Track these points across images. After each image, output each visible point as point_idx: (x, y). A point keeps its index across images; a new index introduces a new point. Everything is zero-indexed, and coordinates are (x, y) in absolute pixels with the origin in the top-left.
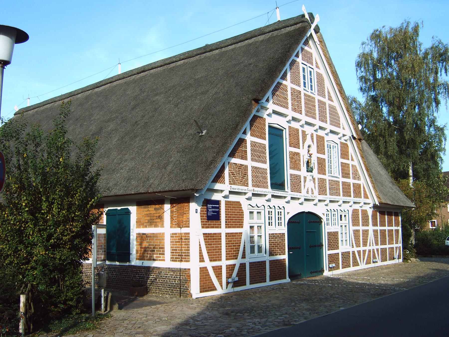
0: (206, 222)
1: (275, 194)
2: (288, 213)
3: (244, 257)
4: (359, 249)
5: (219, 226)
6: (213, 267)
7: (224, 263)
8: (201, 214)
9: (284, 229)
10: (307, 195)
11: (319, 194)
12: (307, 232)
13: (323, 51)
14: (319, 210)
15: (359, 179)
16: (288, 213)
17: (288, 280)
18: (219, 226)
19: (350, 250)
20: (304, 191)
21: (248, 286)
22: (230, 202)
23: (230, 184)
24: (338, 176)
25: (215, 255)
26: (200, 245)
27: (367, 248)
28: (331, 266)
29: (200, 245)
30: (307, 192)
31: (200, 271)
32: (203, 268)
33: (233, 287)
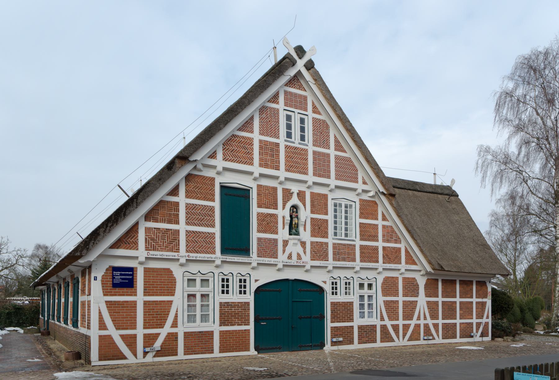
0: (110, 289)
1: (261, 262)
3: (419, 318)
4: (426, 322)
6: (392, 325)
7: (440, 321)
8: (102, 281)
9: (250, 298)
10: (290, 261)
11: (312, 260)
12: (293, 301)
13: (321, 90)
14: (316, 278)
15: (398, 241)
16: (256, 281)
17: (252, 352)
19: (378, 323)
22: (149, 268)
23: (146, 250)
24: (354, 239)
25: (434, 316)
26: (177, 311)
28: (334, 340)
29: (177, 311)
31: (144, 337)
32: (384, 325)
33: (154, 356)
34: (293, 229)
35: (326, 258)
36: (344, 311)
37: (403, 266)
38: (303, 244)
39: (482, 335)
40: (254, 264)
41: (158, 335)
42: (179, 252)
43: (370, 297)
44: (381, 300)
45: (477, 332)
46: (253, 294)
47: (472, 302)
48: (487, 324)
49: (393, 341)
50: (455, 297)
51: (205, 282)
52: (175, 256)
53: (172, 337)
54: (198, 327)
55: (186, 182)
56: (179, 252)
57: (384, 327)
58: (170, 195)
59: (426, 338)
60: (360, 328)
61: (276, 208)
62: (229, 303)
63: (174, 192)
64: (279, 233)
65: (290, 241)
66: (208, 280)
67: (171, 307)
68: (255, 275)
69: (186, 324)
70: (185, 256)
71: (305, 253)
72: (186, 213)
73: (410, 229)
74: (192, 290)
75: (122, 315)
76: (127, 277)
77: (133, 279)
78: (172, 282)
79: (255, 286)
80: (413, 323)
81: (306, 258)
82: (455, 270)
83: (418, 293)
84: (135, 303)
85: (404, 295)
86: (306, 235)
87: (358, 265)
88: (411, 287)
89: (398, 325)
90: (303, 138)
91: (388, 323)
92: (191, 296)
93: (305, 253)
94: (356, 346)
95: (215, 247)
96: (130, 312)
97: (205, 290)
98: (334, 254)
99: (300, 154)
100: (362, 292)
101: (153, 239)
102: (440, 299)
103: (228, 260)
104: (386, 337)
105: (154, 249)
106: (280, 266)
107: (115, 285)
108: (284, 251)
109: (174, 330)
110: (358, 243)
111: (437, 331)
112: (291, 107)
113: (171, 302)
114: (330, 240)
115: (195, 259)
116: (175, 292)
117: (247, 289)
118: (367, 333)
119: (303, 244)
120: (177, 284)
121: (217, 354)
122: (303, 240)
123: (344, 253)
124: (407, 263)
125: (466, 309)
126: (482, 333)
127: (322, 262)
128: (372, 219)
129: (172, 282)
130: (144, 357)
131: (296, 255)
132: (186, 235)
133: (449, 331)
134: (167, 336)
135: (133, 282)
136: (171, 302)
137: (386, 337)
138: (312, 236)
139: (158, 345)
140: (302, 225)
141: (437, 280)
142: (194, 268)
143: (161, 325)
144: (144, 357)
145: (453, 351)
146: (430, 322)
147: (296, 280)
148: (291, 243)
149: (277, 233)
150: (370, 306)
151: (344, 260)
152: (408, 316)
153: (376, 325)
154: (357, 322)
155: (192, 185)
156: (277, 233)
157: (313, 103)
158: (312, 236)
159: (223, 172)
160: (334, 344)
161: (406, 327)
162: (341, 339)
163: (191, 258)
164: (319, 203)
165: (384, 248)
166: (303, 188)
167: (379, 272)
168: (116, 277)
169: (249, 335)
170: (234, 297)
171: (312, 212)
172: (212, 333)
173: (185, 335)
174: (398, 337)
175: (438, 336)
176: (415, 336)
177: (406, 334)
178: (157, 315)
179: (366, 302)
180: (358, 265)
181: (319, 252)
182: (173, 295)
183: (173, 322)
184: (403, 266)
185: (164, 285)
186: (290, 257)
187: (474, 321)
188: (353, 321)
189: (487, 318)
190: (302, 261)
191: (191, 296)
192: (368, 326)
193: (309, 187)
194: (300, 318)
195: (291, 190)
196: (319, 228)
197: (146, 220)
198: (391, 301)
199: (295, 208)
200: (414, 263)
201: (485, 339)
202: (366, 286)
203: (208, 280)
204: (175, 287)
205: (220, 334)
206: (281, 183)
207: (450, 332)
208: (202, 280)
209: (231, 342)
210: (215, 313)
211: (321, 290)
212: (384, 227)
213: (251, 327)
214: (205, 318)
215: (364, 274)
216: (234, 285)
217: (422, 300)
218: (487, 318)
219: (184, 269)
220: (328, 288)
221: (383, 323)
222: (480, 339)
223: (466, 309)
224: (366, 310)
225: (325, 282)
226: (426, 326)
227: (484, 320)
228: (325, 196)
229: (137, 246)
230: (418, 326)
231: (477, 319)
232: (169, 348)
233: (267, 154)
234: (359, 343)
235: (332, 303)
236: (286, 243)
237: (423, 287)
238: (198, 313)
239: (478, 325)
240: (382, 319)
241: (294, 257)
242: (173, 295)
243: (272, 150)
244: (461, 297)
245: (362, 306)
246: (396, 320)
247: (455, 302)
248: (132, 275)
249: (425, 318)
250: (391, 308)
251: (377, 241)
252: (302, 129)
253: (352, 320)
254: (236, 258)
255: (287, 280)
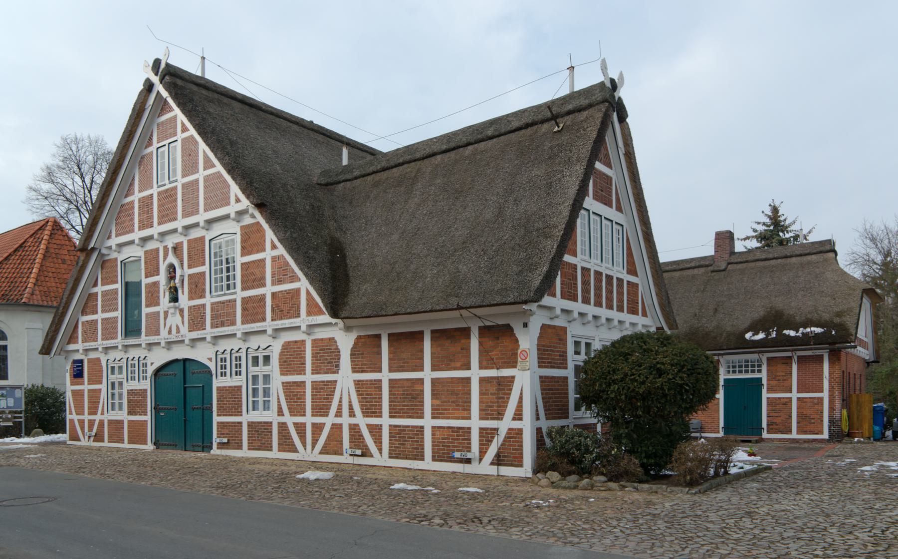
2: (152, 364)
3: (339, 413)
4: (353, 421)
5: (83, 384)
7: (386, 421)
9: (146, 385)
10: (170, 336)
14: (203, 354)
17: (150, 447)
18: (83, 384)
20: (164, 333)
21: (106, 444)
25: (371, 408)
26: (521, 394)
27: (98, 418)
29: (521, 394)
30: (170, 332)
32: (355, 425)
36: (232, 400)
49: (295, 450)
53: (515, 436)
57: (283, 426)
71: (183, 323)
79: (151, 370)
80: (329, 421)
83: (338, 366)
85: (315, 371)
89: (304, 425)
92: (255, 378)
93: (183, 323)
100: (253, 370)
102: (385, 376)
104: (286, 444)
111: (378, 442)
118: (260, 435)
122: (181, 307)
126: (498, 455)
133: (406, 443)
137: (286, 444)
141: (378, 337)
145: (374, 487)
146: (362, 421)
150: (266, 392)
152: (321, 409)
153: (271, 423)
161: (318, 428)
174: (305, 446)
175: (380, 450)
177: (317, 440)
179: (260, 386)
183: (516, 410)
192: (260, 423)
194: (193, 409)
198: (294, 382)
201: (508, 471)
207: (408, 445)
214: (266, 407)
217: (346, 379)
221: (282, 419)
222: (493, 470)
224: (261, 399)
225: (210, 359)
226: (355, 430)
237: (349, 352)
241: (174, 331)
249: (352, 414)
250: (293, 392)
253: (239, 413)
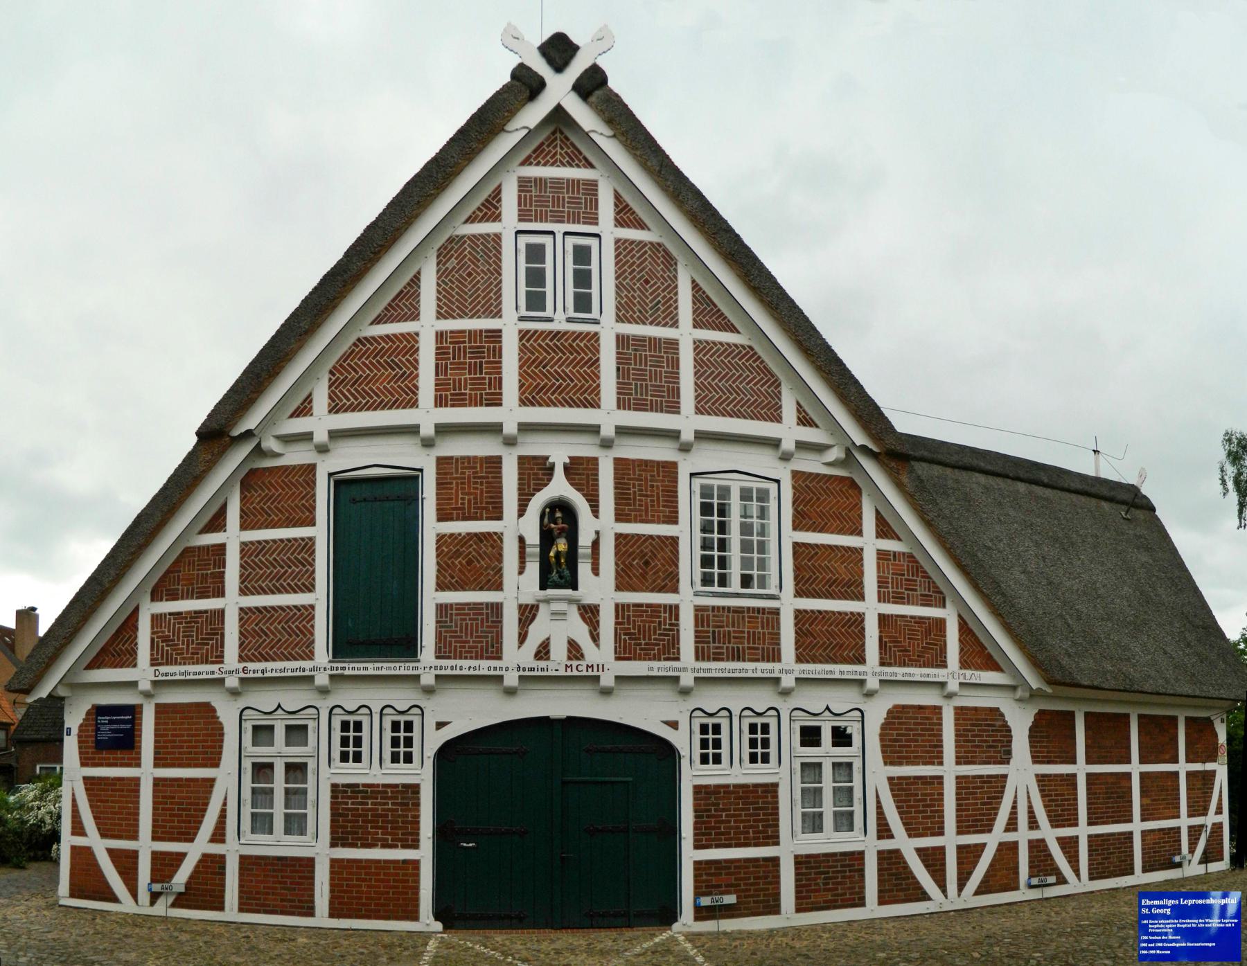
3: (1012, 825)
7: (1083, 831)
8: (79, 736)
9: (422, 774)
10: (542, 664)
11: (618, 659)
14: (643, 712)
15: (936, 596)
17: (427, 921)
19: (871, 846)
23: (152, 665)
25: (1062, 814)
26: (225, 804)
28: (705, 901)
34: (559, 570)
35: (670, 651)
36: (749, 812)
37: (952, 672)
38: (590, 614)
39: (1205, 860)
40: (428, 679)
41: (181, 856)
42: (222, 662)
43: (843, 768)
44: (878, 774)
45: (1192, 851)
46: (429, 764)
47: (1176, 774)
48: (1218, 827)
49: (924, 896)
50: (1128, 761)
51: (297, 733)
52: (212, 673)
54: (278, 844)
55: (242, 493)
56: (222, 662)
58: (207, 532)
59: (1035, 881)
60: (802, 862)
61: (496, 513)
62: (357, 785)
63: (217, 522)
64: (505, 586)
65: (542, 607)
66: (305, 727)
67: (211, 792)
68: (436, 708)
69: (248, 836)
70: (237, 671)
71: (595, 638)
72: (242, 566)
73: (966, 561)
74: (263, 753)
75: (114, 807)
76: (122, 726)
77: (133, 729)
78: (215, 735)
79: (434, 741)
80: (992, 840)
81: (601, 654)
82: (1112, 684)
83: (1009, 753)
84: (136, 781)
86: (599, 586)
87: (791, 672)
88: (982, 733)
89: (941, 850)
90: (583, 303)
91: (907, 845)
92: (262, 770)
93: (595, 638)
94: (789, 916)
95: (313, 642)
96: (127, 802)
97: (296, 753)
98: (699, 638)
99: (572, 349)
101: (166, 639)
102: (1081, 769)
103: (347, 672)
105: (169, 662)
106: (511, 679)
107: (100, 745)
108: (522, 638)
109: (216, 849)
110: (789, 604)
111: (1073, 860)
112: (541, 218)
113: (211, 782)
114: (688, 598)
115: (260, 675)
116: (220, 759)
117: (415, 750)
118: (829, 879)
119: (590, 614)
120: (226, 738)
121: (322, 918)
122: (589, 600)
123: (737, 636)
124: (965, 664)
125: (1160, 795)
126: (1205, 853)
127: (655, 664)
128: (840, 531)
129: (215, 735)
130: (152, 903)
131: (565, 646)
132: (241, 619)
133: (1111, 855)
134: (200, 861)
135: (133, 735)
136: (211, 782)
137: (898, 883)
138: (619, 588)
139: (181, 877)
140: (585, 556)
142: (264, 700)
143: (189, 834)
144: (152, 903)
146: (1050, 834)
147: (570, 719)
148: (543, 612)
149: (499, 587)
151: (736, 656)
154: (793, 844)
155: (256, 495)
156: (499, 587)
157: (617, 197)
158: (619, 588)
159: (334, 442)
160: (702, 913)
161: (969, 856)
162: (730, 899)
163: (251, 675)
164: (646, 489)
165: (883, 619)
166: (583, 448)
167: (869, 695)
168: (102, 728)
169: (418, 875)
170: (376, 771)
171: (620, 517)
172: (309, 863)
173: (241, 863)
176: (1002, 875)
177: (970, 874)
178: (181, 810)
180: (791, 672)
181: (645, 635)
182: (217, 765)
184: (952, 672)
185: (197, 741)
186: (543, 652)
187: (1184, 822)
188: (777, 844)
189: (1219, 811)
190: (584, 663)
191: (262, 770)
192: (834, 854)
193: (607, 444)
195: (547, 458)
196: (647, 563)
197: (153, 600)
199: (561, 513)
200: (993, 666)
201: (1214, 867)
202: (827, 736)
203: (305, 727)
204: (221, 747)
205: (332, 867)
206: (510, 442)
208: (288, 728)
209: (365, 892)
210: (321, 815)
211: (667, 752)
212: (882, 555)
213: (424, 854)
214: (295, 824)
215: (814, 700)
216: (376, 738)
217: (1022, 773)
218: (1219, 811)
219: (242, 703)
220: (684, 741)
223: (1160, 795)
225: (674, 725)
226: (1038, 848)
227: (1210, 819)
228: (670, 469)
229: (135, 659)
230: (1007, 851)
231: (1189, 816)
232: (204, 889)
233: (459, 367)
234: (798, 910)
235: (698, 790)
236: (528, 614)
238: (279, 810)
239: (1195, 832)
240: (884, 831)
241: (559, 652)
242: (217, 765)
243: (477, 352)
244: (1143, 761)
245: (812, 796)
246: (933, 835)
247: (1128, 776)
248: (132, 722)
249: (1033, 824)
251: (860, 597)
252: (582, 279)
253: (774, 840)
254: (370, 665)
255: (546, 720)
